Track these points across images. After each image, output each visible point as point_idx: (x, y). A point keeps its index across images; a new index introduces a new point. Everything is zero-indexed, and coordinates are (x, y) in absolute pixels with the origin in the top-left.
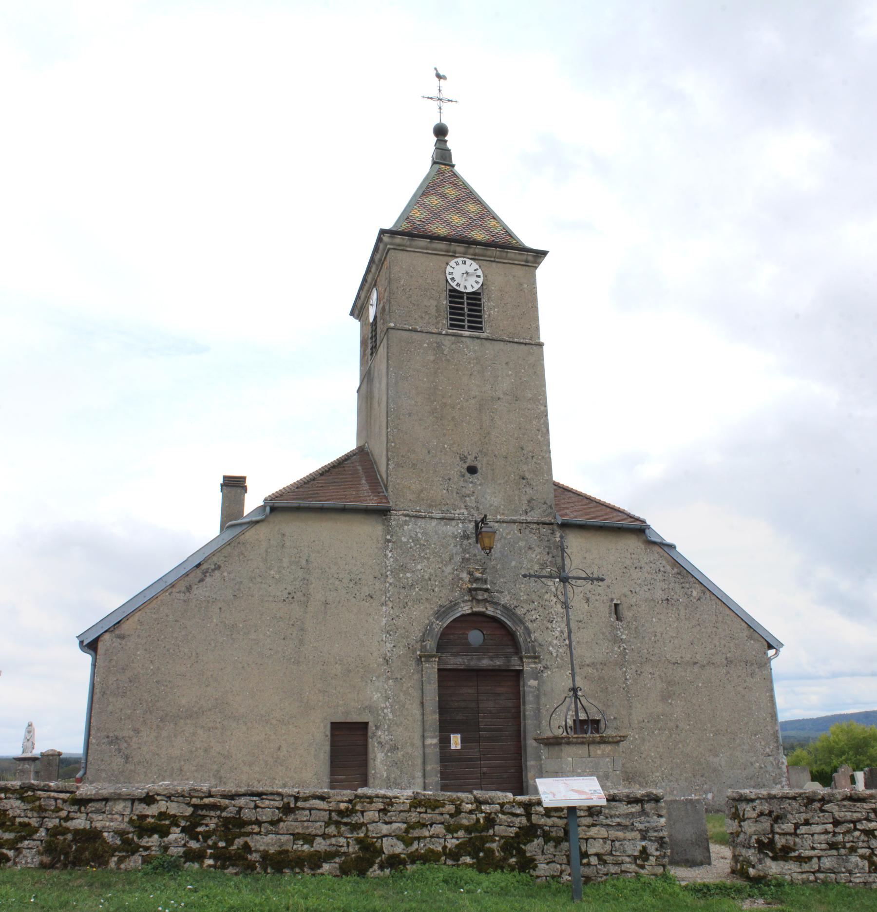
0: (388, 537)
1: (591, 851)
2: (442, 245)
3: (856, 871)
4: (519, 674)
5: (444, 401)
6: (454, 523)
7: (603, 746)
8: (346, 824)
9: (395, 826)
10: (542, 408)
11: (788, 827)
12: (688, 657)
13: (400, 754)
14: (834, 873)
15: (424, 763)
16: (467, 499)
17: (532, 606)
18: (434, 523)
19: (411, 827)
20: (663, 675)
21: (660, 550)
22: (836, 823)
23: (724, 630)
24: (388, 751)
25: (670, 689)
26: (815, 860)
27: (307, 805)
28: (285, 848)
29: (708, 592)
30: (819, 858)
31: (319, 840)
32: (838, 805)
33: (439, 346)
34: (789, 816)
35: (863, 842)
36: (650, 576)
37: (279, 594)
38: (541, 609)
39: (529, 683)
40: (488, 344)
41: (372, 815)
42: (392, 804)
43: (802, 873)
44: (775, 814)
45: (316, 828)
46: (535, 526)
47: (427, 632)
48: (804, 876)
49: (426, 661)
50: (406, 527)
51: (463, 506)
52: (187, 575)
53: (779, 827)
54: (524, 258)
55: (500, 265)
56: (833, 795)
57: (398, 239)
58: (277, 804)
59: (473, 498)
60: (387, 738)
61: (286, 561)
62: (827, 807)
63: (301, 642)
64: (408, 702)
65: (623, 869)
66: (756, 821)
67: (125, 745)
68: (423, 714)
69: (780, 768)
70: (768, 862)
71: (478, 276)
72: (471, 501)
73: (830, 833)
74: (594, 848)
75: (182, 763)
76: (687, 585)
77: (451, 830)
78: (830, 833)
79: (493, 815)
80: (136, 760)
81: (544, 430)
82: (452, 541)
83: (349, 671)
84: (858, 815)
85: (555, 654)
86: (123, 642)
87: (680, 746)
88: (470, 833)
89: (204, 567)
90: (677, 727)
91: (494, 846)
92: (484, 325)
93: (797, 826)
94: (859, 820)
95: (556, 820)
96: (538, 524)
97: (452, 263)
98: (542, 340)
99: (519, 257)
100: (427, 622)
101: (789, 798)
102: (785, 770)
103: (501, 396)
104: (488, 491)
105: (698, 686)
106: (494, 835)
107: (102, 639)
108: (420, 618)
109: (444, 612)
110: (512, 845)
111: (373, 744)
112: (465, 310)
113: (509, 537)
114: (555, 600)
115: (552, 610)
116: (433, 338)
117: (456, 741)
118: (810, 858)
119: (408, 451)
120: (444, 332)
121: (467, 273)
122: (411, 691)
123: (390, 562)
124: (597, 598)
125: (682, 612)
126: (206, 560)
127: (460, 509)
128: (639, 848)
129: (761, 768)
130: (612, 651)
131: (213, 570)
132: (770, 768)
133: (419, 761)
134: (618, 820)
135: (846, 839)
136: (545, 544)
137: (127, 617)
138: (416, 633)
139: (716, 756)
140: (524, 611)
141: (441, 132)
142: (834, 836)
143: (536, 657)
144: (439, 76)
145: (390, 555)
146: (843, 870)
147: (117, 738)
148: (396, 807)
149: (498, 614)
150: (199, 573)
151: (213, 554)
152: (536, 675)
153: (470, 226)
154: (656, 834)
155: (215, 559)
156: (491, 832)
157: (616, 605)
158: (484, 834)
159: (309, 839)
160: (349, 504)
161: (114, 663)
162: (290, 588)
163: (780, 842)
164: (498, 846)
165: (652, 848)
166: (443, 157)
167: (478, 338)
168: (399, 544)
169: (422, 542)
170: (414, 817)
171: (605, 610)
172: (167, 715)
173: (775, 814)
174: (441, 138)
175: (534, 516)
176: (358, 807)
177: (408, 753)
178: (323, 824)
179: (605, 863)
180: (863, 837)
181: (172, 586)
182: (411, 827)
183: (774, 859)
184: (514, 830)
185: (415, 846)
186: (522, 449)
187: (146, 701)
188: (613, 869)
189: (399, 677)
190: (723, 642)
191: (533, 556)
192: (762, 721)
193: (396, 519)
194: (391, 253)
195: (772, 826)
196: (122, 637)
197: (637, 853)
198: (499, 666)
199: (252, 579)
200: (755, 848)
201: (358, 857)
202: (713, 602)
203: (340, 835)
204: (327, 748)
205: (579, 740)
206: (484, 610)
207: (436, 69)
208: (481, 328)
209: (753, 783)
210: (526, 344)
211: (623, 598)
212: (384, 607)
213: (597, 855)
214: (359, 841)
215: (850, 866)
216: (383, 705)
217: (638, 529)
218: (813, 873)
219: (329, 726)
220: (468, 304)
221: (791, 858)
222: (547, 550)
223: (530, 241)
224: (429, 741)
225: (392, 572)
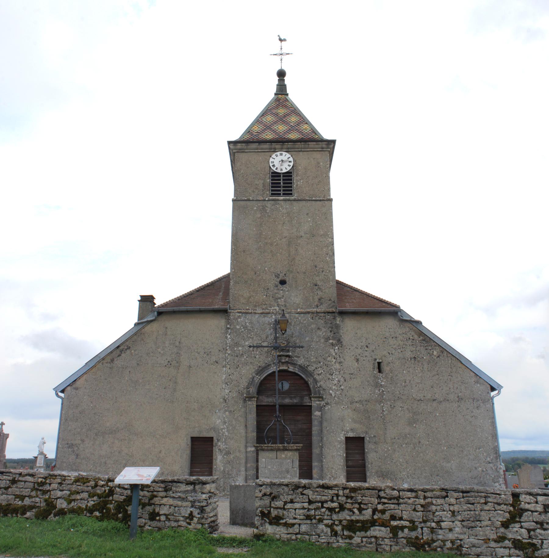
0: (228, 326)
1: (161, 513)
2: (267, 146)
3: (322, 534)
5: (266, 241)
6: (270, 315)
7: (286, 452)
8: (40, 490)
9: (65, 492)
10: (330, 240)
11: (279, 504)
12: (429, 396)
13: (232, 457)
14: (308, 535)
15: (246, 463)
16: (279, 300)
18: (257, 316)
19: (72, 493)
20: (410, 408)
21: (410, 325)
22: (310, 502)
23: (457, 378)
24: (224, 455)
25: (415, 417)
26: (297, 526)
27: (23, 479)
28: (9, 502)
29: (445, 352)
30: (300, 525)
31: (27, 499)
32: (312, 491)
33: (264, 208)
34: (281, 497)
35: (328, 515)
36: (402, 343)
37: (163, 362)
38: (325, 367)
40: (295, 203)
41: (55, 486)
42: (64, 480)
43: (288, 534)
44: (273, 495)
45: (26, 492)
46: (322, 315)
47: (251, 382)
48: (289, 536)
49: (249, 400)
50: (239, 320)
51: (276, 305)
52: (111, 352)
53: (274, 504)
54: (320, 146)
55: (305, 153)
56: (311, 484)
57: (239, 146)
58: (9, 478)
59: (283, 300)
60: (224, 447)
61: (167, 343)
62: (305, 492)
63: (175, 390)
64: (238, 425)
65: (179, 524)
66: (261, 499)
67: (76, 448)
68: (246, 433)
69: (498, 472)
70: (267, 525)
71: (290, 162)
72: (281, 302)
73: (306, 509)
74: (164, 510)
75: (106, 459)
76: (430, 348)
77: (91, 495)
78: (306, 509)
79: (113, 488)
80: (82, 457)
81: (331, 254)
82: (268, 326)
83: (202, 407)
84: (326, 498)
86: (77, 392)
87: (422, 455)
88: (100, 498)
89: (121, 348)
90: (420, 442)
91: (111, 506)
92: (292, 192)
93: (285, 503)
94: (326, 502)
95: (146, 493)
96: (325, 313)
97: (274, 156)
98: (332, 197)
99: (317, 146)
100: (251, 376)
101: (284, 485)
102: (502, 473)
103: (303, 235)
104: (293, 294)
105: (436, 415)
106: (113, 500)
107: (66, 390)
108: (247, 373)
109: (261, 370)
110: (121, 507)
111: (216, 450)
112: (282, 184)
113: (305, 322)
114: (334, 361)
115: (333, 367)
116: (260, 204)
118: (293, 525)
119: (243, 273)
120: (267, 199)
121: (282, 161)
122: (240, 418)
123: (229, 341)
124: (365, 358)
125: (426, 366)
126: (122, 344)
127: (274, 307)
128: (189, 512)
129: (483, 471)
130: (374, 393)
131: (126, 349)
132: (490, 472)
133: (243, 461)
134: (179, 494)
135: (317, 513)
136: (329, 325)
137: (79, 378)
138: (244, 383)
139: (449, 462)
140: (313, 368)
141: (281, 74)
142: (308, 511)
143: (319, 397)
144: (281, 40)
145: (229, 337)
146: (314, 533)
147: (72, 445)
148: (67, 482)
149: (297, 371)
150: (118, 351)
151: (127, 340)
152: (320, 409)
153: (288, 131)
154: (199, 504)
155: (127, 343)
156: (111, 498)
157: (379, 364)
158: (107, 499)
159: (22, 498)
160: (203, 308)
161: (72, 403)
162: (169, 359)
163: (274, 513)
164: (114, 506)
165: (196, 512)
166: (282, 89)
167: (289, 200)
168: (235, 330)
169: (249, 328)
170: (74, 488)
171: (369, 367)
172: (99, 432)
173: (273, 495)
174: (281, 78)
175: (322, 308)
176: (48, 481)
177: (236, 456)
178: (30, 490)
179: (169, 520)
180: (327, 513)
181: (103, 359)
182: (72, 493)
183: (271, 523)
184: (123, 497)
185: (73, 504)
186: (316, 267)
187: (88, 424)
188: (174, 524)
189: (232, 410)
190: (456, 386)
191: (321, 333)
192: (485, 439)
193: (234, 314)
194: (236, 155)
195: (271, 502)
196: (77, 389)
197: (187, 515)
198: (296, 403)
199: (148, 354)
200: (259, 516)
201: (44, 510)
202: (449, 358)
203: (37, 496)
204: (188, 452)
205: (269, 448)
206: (286, 368)
207: (279, 36)
208: (291, 194)
209: (476, 481)
210: (320, 200)
211: (384, 358)
212: (224, 369)
213: (165, 515)
214: (46, 500)
215: (318, 531)
216: (222, 427)
217: (392, 312)
218: (296, 534)
219: (189, 440)
220: (283, 180)
221: (281, 524)
222: (330, 329)
223: (327, 135)
224: (249, 449)
225: (230, 347)
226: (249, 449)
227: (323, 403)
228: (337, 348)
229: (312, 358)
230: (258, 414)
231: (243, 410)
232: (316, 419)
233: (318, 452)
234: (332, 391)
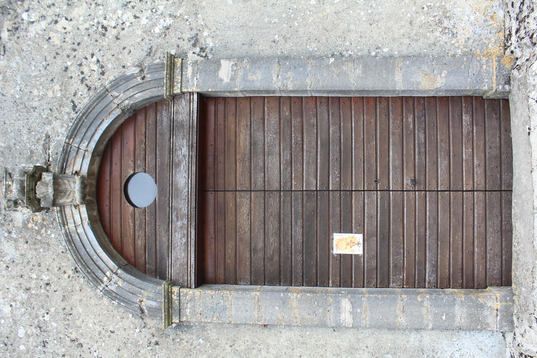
4: (204, 100)
15: (392, 328)
17: (74, 71)
38: (80, 53)
39: (226, 80)
68: (289, 326)
85: (169, 21)
109: (86, 266)
114: (63, 22)
115: (82, 28)
117: (347, 244)
138: (126, 324)
140: (82, 89)
143: (172, 66)
149: (89, 145)
152: (210, 61)
198: (190, 147)
226: (346, 317)
227: (191, 57)
228: (25, 16)
229: (50, 94)
230: (231, 279)
231: (213, 334)
232: (245, 75)
233: (359, 71)
234: (154, 25)
